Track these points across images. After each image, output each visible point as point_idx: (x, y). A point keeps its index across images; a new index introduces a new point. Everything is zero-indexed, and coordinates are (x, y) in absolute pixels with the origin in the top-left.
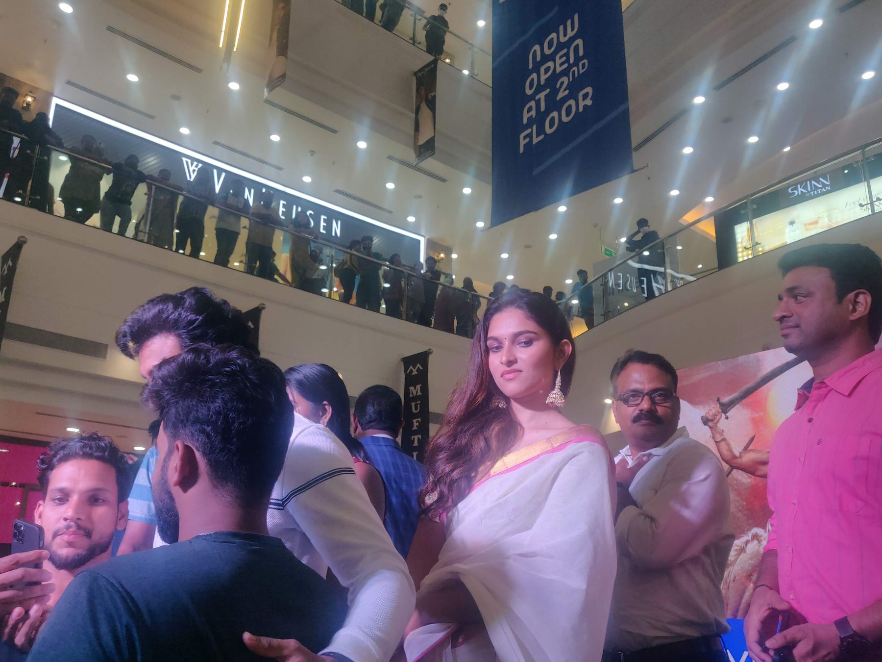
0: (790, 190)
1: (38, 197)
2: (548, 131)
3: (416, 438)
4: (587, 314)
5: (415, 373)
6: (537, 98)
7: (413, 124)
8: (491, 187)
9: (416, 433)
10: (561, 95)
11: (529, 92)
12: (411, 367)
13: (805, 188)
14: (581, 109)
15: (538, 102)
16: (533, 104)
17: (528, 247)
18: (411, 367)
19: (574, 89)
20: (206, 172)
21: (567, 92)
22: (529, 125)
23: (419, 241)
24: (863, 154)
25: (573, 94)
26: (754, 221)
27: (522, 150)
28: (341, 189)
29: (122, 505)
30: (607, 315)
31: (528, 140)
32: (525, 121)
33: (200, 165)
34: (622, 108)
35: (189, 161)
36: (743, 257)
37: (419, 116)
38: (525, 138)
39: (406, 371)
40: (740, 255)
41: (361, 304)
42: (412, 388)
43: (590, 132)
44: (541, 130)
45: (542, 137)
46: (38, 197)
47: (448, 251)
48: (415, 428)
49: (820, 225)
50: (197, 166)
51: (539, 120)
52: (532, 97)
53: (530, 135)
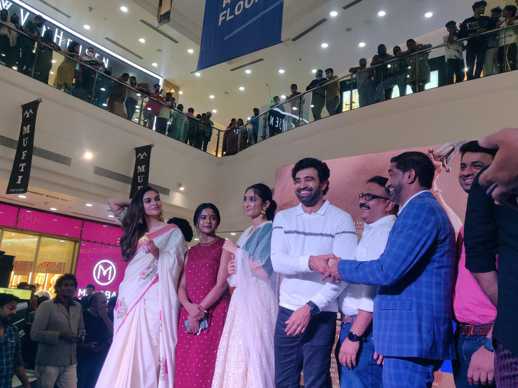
1: (39, 73)
2: (237, 13)
3: (23, 165)
5: (142, 158)
8: (199, 47)
9: (22, 162)
12: (140, 154)
18: (140, 154)
22: (226, 9)
23: (159, 80)
29: (365, 288)
31: (224, 17)
32: (224, 6)
38: (223, 16)
39: (136, 156)
42: (139, 167)
44: (232, 13)
45: (233, 16)
46: (39, 73)
47: (177, 88)
50: (8, 4)
53: (225, 15)
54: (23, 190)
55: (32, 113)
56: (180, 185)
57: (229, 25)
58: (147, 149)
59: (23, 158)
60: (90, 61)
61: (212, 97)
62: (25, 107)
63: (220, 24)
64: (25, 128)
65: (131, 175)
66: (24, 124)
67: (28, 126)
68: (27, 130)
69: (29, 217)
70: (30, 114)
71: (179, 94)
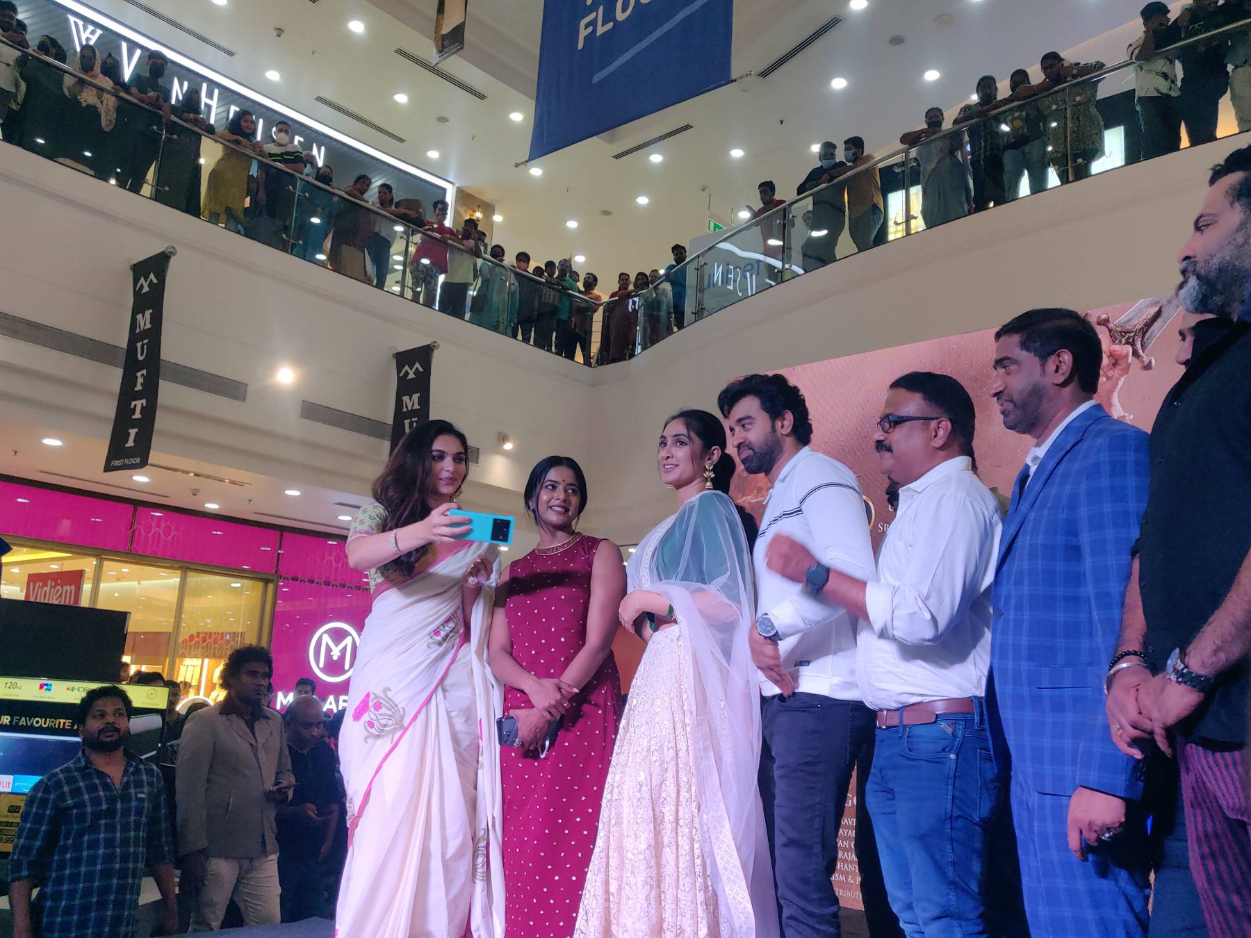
2: (620, 16)
3: (139, 404)
5: (411, 376)
9: (138, 396)
12: (407, 368)
17: (606, 213)
18: (407, 368)
20: (156, 67)
27: (580, 45)
31: (590, 29)
33: (99, 32)
35: (81, 23)
38: (587, 26)
39: (399, 372)
41: (536, 344)
42: (406, 399)
45: (610, 25)
47: (488, 209)
48: (139, 387)
50: (93, 33)
53: (593, 23)
54: (138, 460)
55: (155, 281)
56: (503, 438)
57: (604, 47)
58: (423, 355)
60: (282, 154)
61: (572, 224)
62: (140, 270)
63: (580, 46)
64: (139, 317)
66: (138, 309)
67: (148, 313)
68: (144, 321)
69: (158, 526)
70: (151, 284)
71: (493, 222)
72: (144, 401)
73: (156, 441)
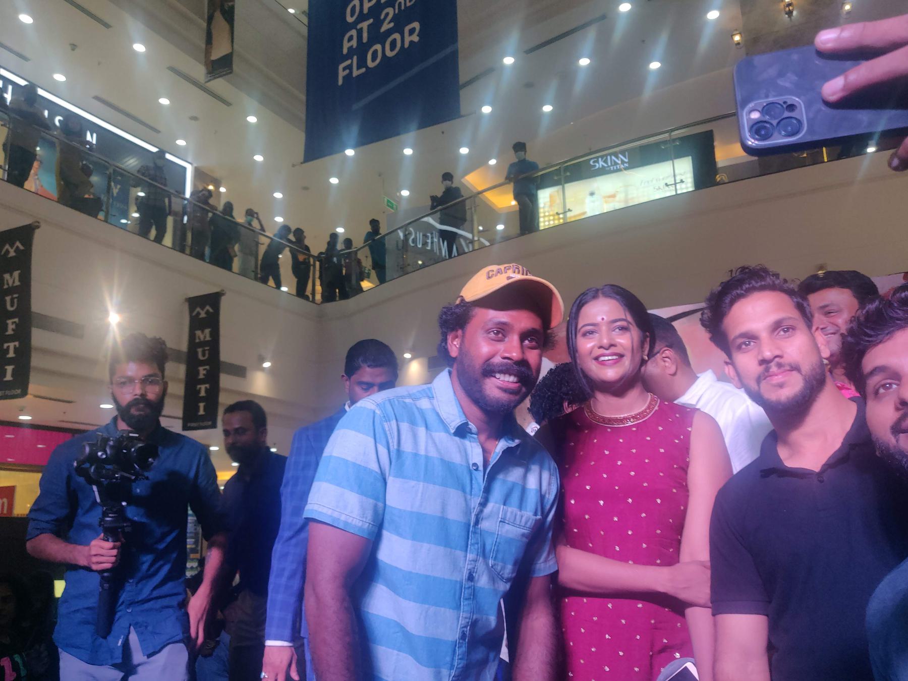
0: (591, 162)
2: (370, 64)
4: (380, 267)
6: (359, 27)
7: (204, 36)
10: (385, 27)
11: (350, 19)
13: (606, 162)
14: (406, 45)
15: (360, 33)
16: (354, 32)
17: (306, 188)
18: (7, 247)
19: (400, 23)
21: (392, 25)
22: (349, 56)
24: (670, 136)
25: (399, 28)
26: (566, 185)
27: (340, 82)
28: (104, 96)
30: (403, 270)
31: (347, 71)
32: (345, 51)
34: (448, 50)
36: (544, 222)
37: (212, 27)
38: (344, 69)
40: (541, 220)
42: (198, 333)
43: (416, 70)
44: (362, 63)
45: (363, 70)
47: (217, 185)
49: (617, 198)
51: (361, 51)
52: (353, 26)
53: (350, 67)
55: (21, 248)
56: (262, 360)
58: (213, 300)
59: (10, 332)
65: (184, 347)
70: (207, 312)
72: (17, 343)
73: (33, 378)
